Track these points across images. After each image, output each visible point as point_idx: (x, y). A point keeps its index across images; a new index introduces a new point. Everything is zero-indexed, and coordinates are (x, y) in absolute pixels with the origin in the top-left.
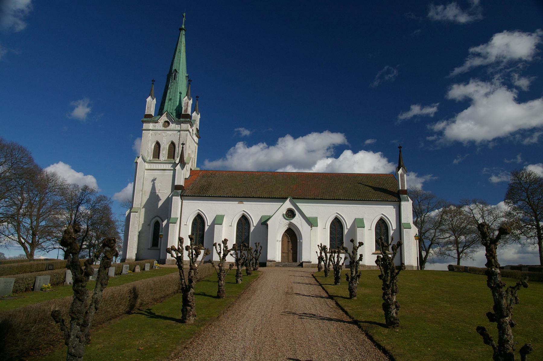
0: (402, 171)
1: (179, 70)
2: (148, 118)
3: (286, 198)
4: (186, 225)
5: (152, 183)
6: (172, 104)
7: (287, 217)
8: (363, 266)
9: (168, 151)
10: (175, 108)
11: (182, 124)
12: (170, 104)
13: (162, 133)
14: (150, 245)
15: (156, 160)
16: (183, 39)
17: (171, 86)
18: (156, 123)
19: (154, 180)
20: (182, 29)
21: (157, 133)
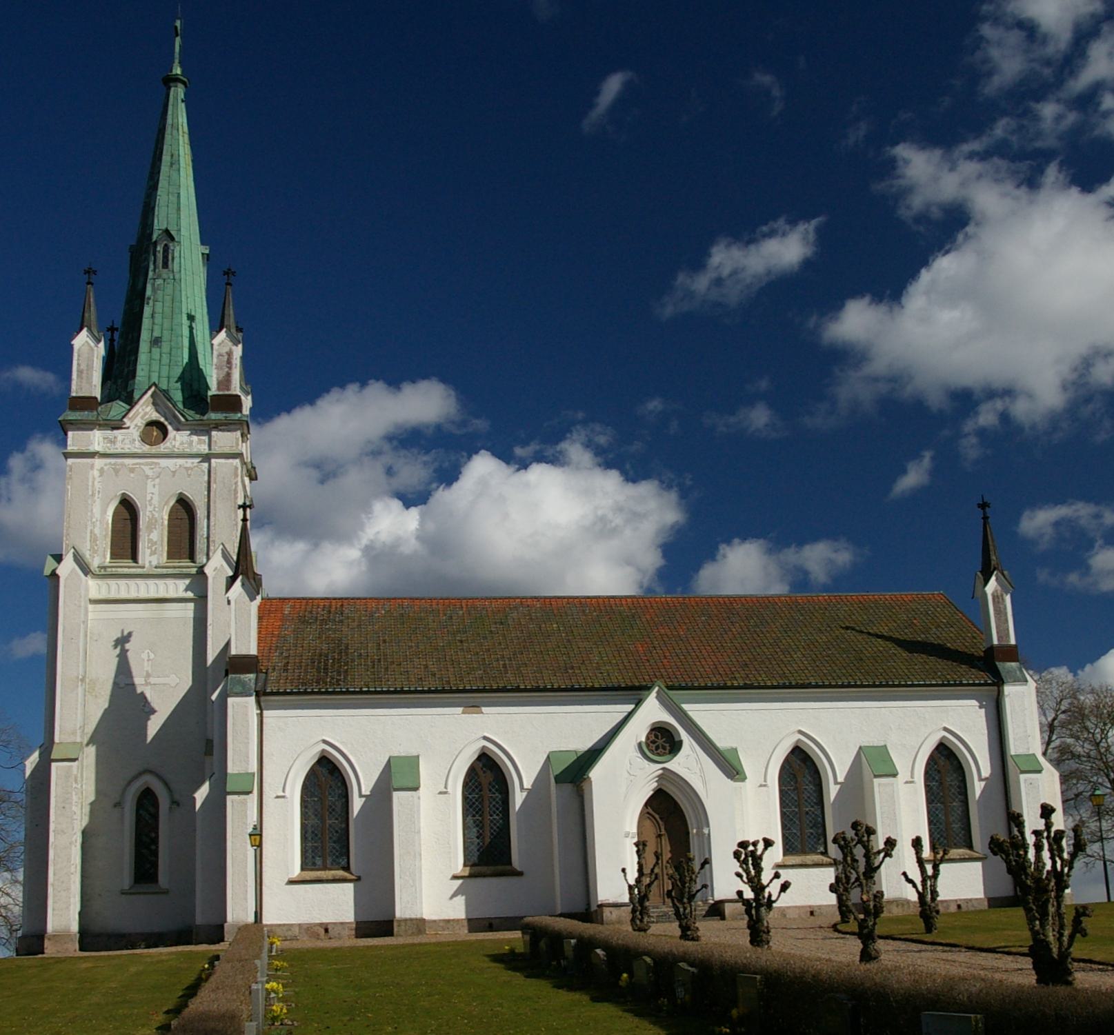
0: (996, 584)
1: (180, 230)
2: (82, 409)
3: (648, 689)
4: (283, 797)
5: (118, 651)
6: (165, 360)
7: (651, 751)
8: (903, 905)
9: (169, 532)
10: (178, 371)
11: (214, 433)
12: (157, 357)
14: (127, 880)
15: (126, 566)
16: (179, 116)
17: (154, 290)
18: (114, 428)
19: (122, 641)
20: (176, 80)
21: (123, 465)
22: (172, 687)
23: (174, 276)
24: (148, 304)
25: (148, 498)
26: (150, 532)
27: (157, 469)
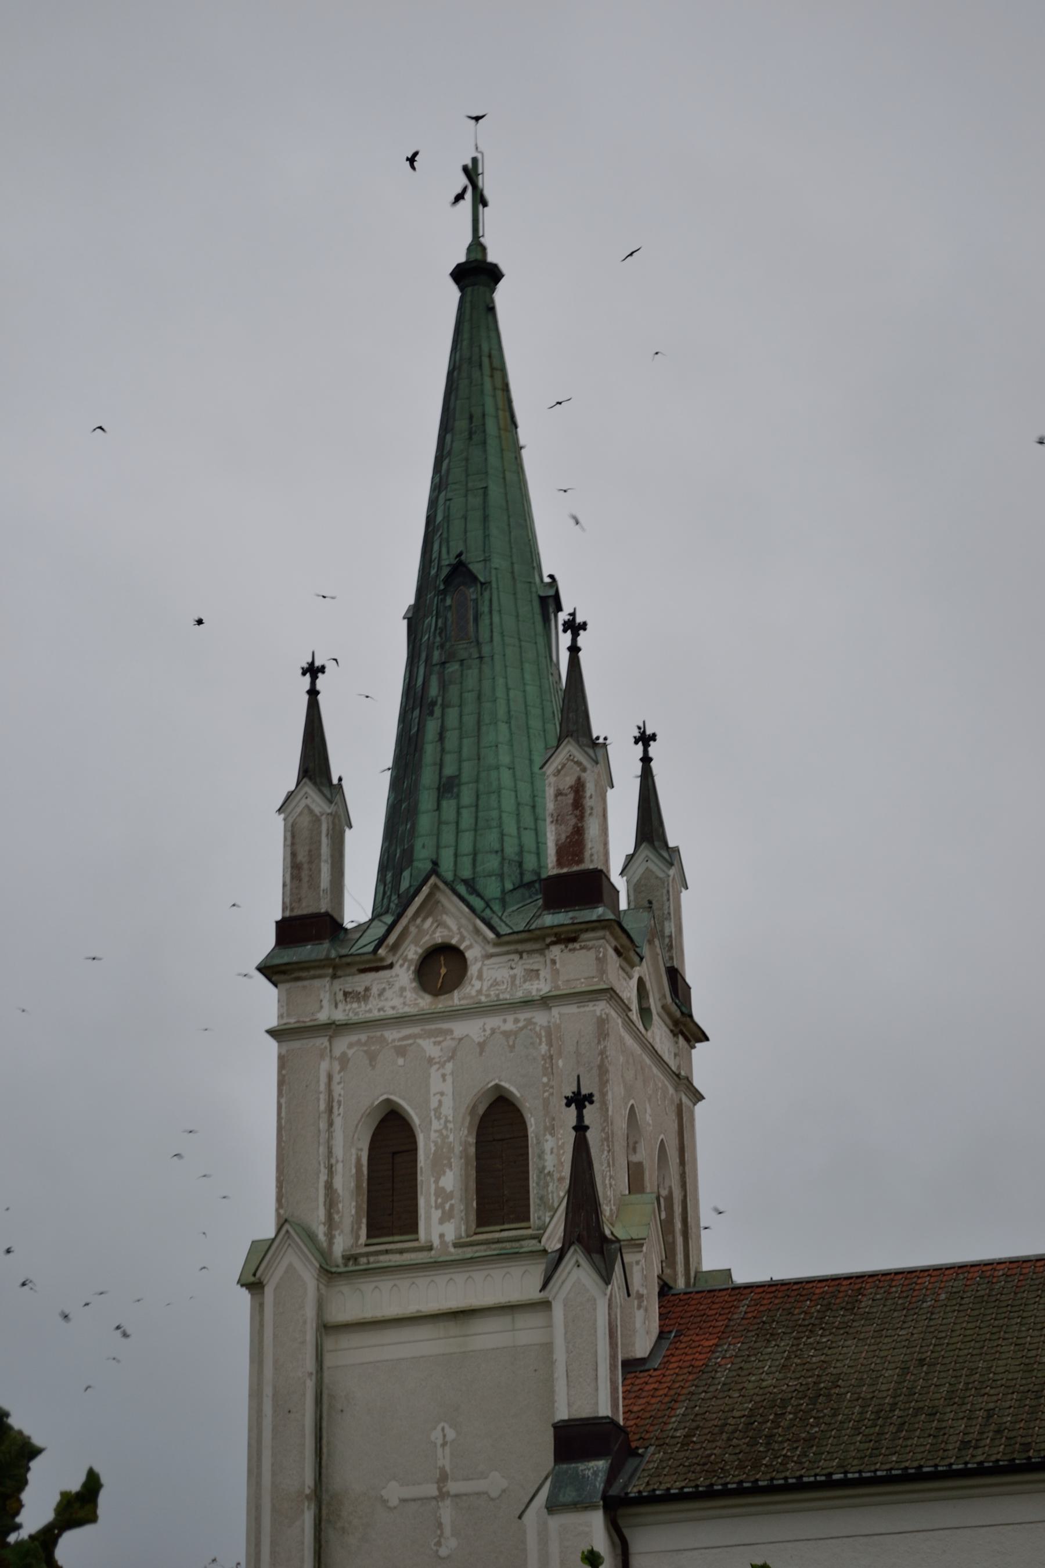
6: (467, 818)
13: (415, 1036)
17: (443, 686)
22: (493, 1499)
23: (480, 652)
24: (431, 713)
25: (434, 1103)
26: (438, 1175)
27: (449, 1043)
